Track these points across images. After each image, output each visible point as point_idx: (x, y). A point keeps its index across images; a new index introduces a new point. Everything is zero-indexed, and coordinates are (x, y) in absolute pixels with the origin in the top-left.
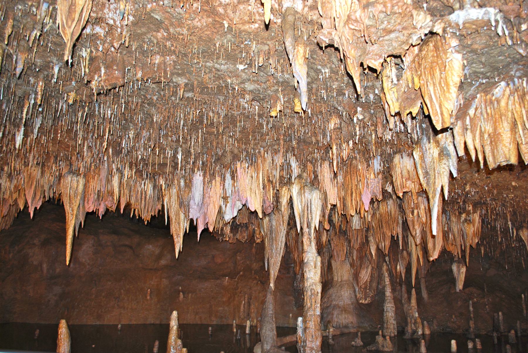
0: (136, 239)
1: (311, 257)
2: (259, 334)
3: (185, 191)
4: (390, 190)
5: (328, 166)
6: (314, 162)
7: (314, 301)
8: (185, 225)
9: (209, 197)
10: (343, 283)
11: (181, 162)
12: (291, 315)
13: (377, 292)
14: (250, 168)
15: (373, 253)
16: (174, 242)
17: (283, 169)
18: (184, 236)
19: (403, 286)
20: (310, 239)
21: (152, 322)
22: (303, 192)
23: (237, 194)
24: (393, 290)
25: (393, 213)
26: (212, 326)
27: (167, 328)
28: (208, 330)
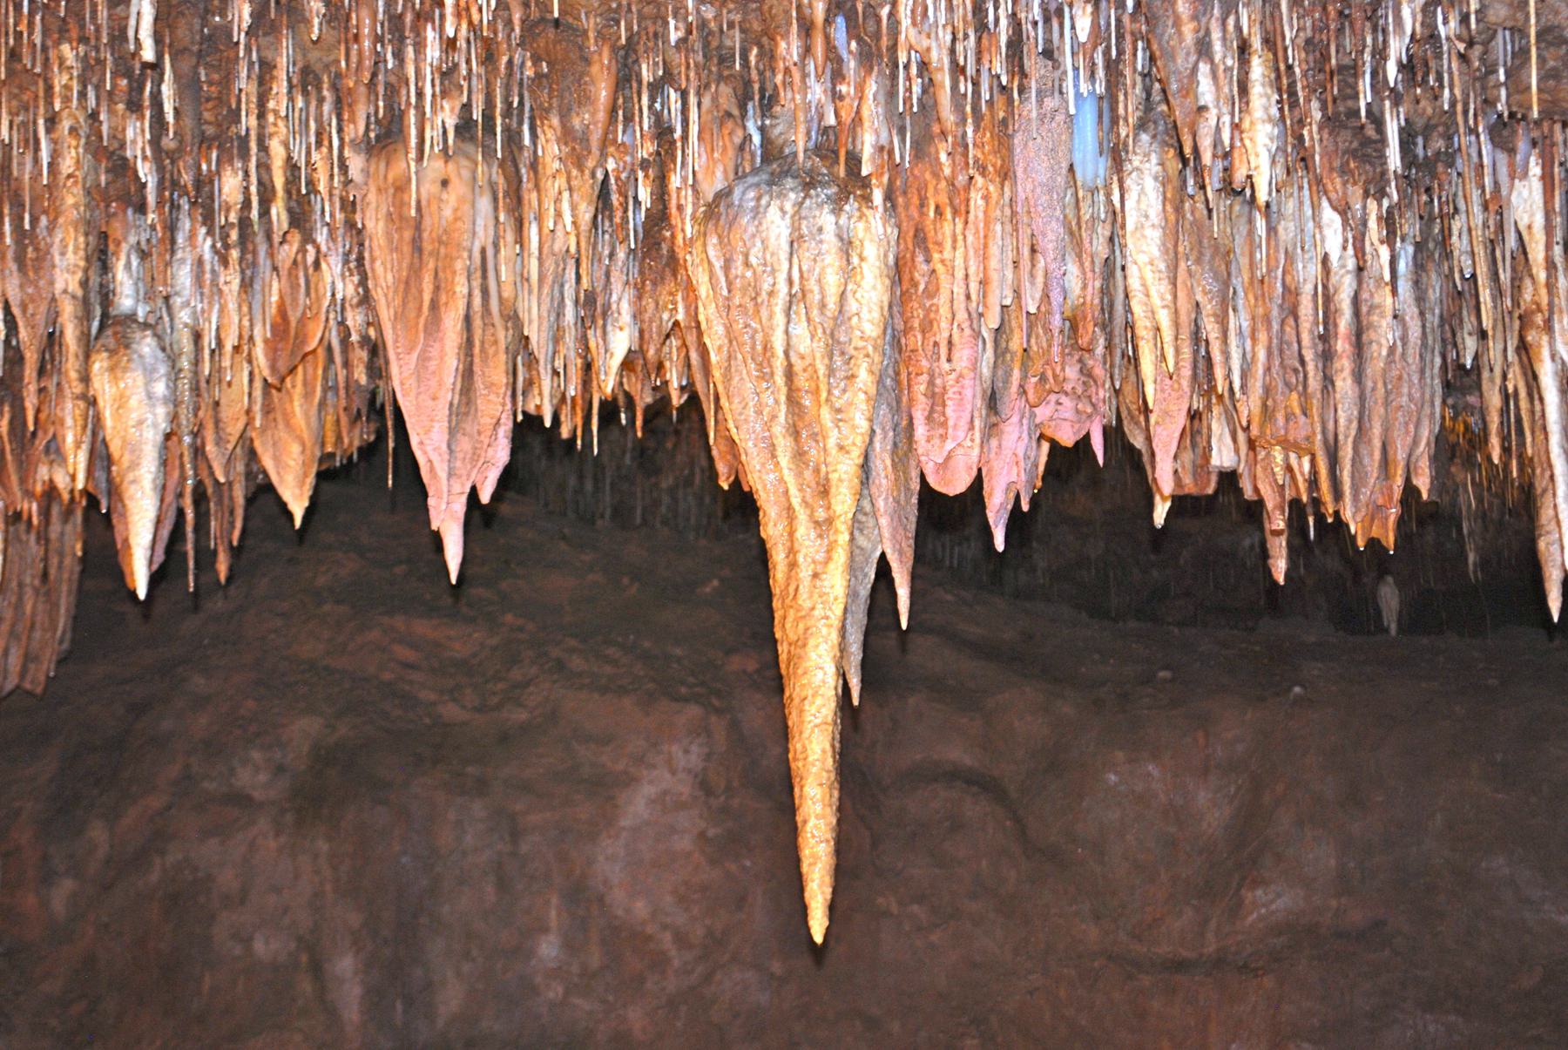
0: (1026, 715)
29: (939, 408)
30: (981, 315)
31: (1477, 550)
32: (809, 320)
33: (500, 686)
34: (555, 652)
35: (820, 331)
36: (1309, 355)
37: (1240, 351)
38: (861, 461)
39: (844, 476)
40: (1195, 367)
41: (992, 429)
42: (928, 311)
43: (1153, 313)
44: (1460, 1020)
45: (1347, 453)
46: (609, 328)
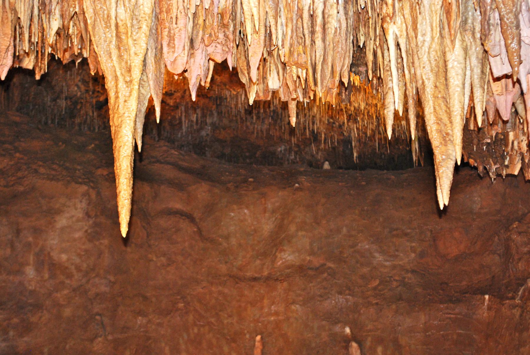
0: (202, 191)
29: (172, 42)
30: (188, 9)
31: (357, 152)
32: (124, 6)
33: (14, 178)
34: (34, 167)
35: (128, 10)
36: (306, 32)
37: (282, 31)
38: (143, 59)
39: (137, 64)
40: (265, 37)
41: (191, 55)
42: (169, 5)
43: (251, 9)
44: (351, 297)
45: (319, 68)
46: (51, 19)
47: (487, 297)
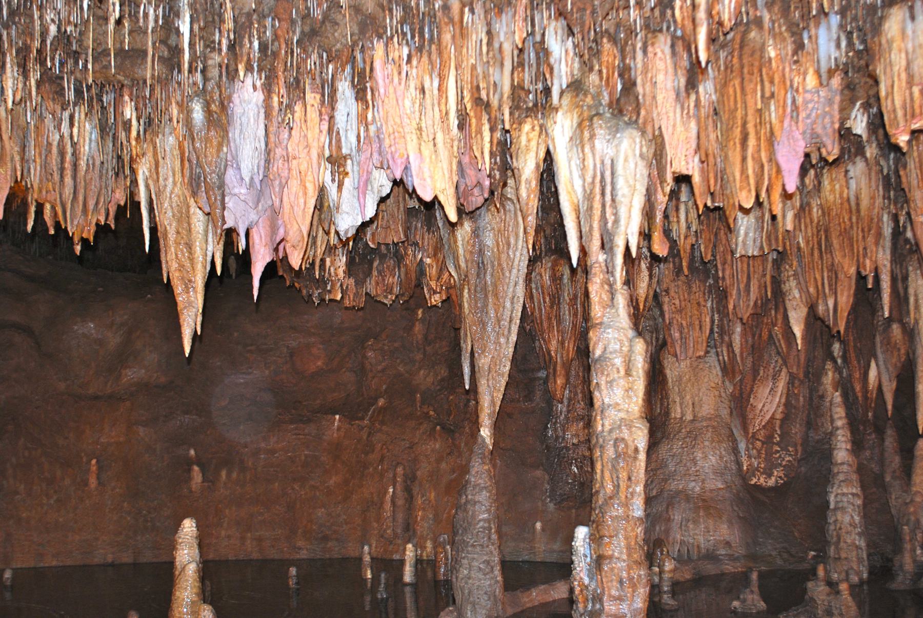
1: (616, 340)
2: (448, 584)
3: (207, 140)
4: (859, 125)
5: (668, 50)
6: (622, 38)
7: (623, 475)
8: (208, 250)
9: (287, 159)
10: (698, 425)
11: (192, 45)
12: (538, 525)
13: (804, 450)
14: (414, 62)
15: (798, 330)
16: (175, 304)
17: (521, 64)
18: (207, 286)
19: (890, 432)
20: (611, 286)
21: (110, 558)
22: (586, 134)
23: (375, 146)
24: (857, 446)
25: (865, 203)
26: (297, 563)
27: (165, 575)
28: (286, 576)
45: (69, 206)
47: (337, 417)
